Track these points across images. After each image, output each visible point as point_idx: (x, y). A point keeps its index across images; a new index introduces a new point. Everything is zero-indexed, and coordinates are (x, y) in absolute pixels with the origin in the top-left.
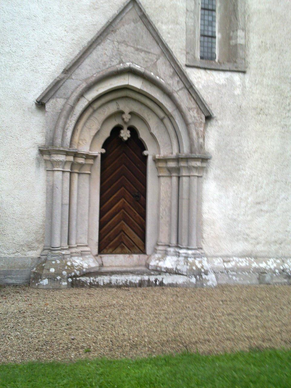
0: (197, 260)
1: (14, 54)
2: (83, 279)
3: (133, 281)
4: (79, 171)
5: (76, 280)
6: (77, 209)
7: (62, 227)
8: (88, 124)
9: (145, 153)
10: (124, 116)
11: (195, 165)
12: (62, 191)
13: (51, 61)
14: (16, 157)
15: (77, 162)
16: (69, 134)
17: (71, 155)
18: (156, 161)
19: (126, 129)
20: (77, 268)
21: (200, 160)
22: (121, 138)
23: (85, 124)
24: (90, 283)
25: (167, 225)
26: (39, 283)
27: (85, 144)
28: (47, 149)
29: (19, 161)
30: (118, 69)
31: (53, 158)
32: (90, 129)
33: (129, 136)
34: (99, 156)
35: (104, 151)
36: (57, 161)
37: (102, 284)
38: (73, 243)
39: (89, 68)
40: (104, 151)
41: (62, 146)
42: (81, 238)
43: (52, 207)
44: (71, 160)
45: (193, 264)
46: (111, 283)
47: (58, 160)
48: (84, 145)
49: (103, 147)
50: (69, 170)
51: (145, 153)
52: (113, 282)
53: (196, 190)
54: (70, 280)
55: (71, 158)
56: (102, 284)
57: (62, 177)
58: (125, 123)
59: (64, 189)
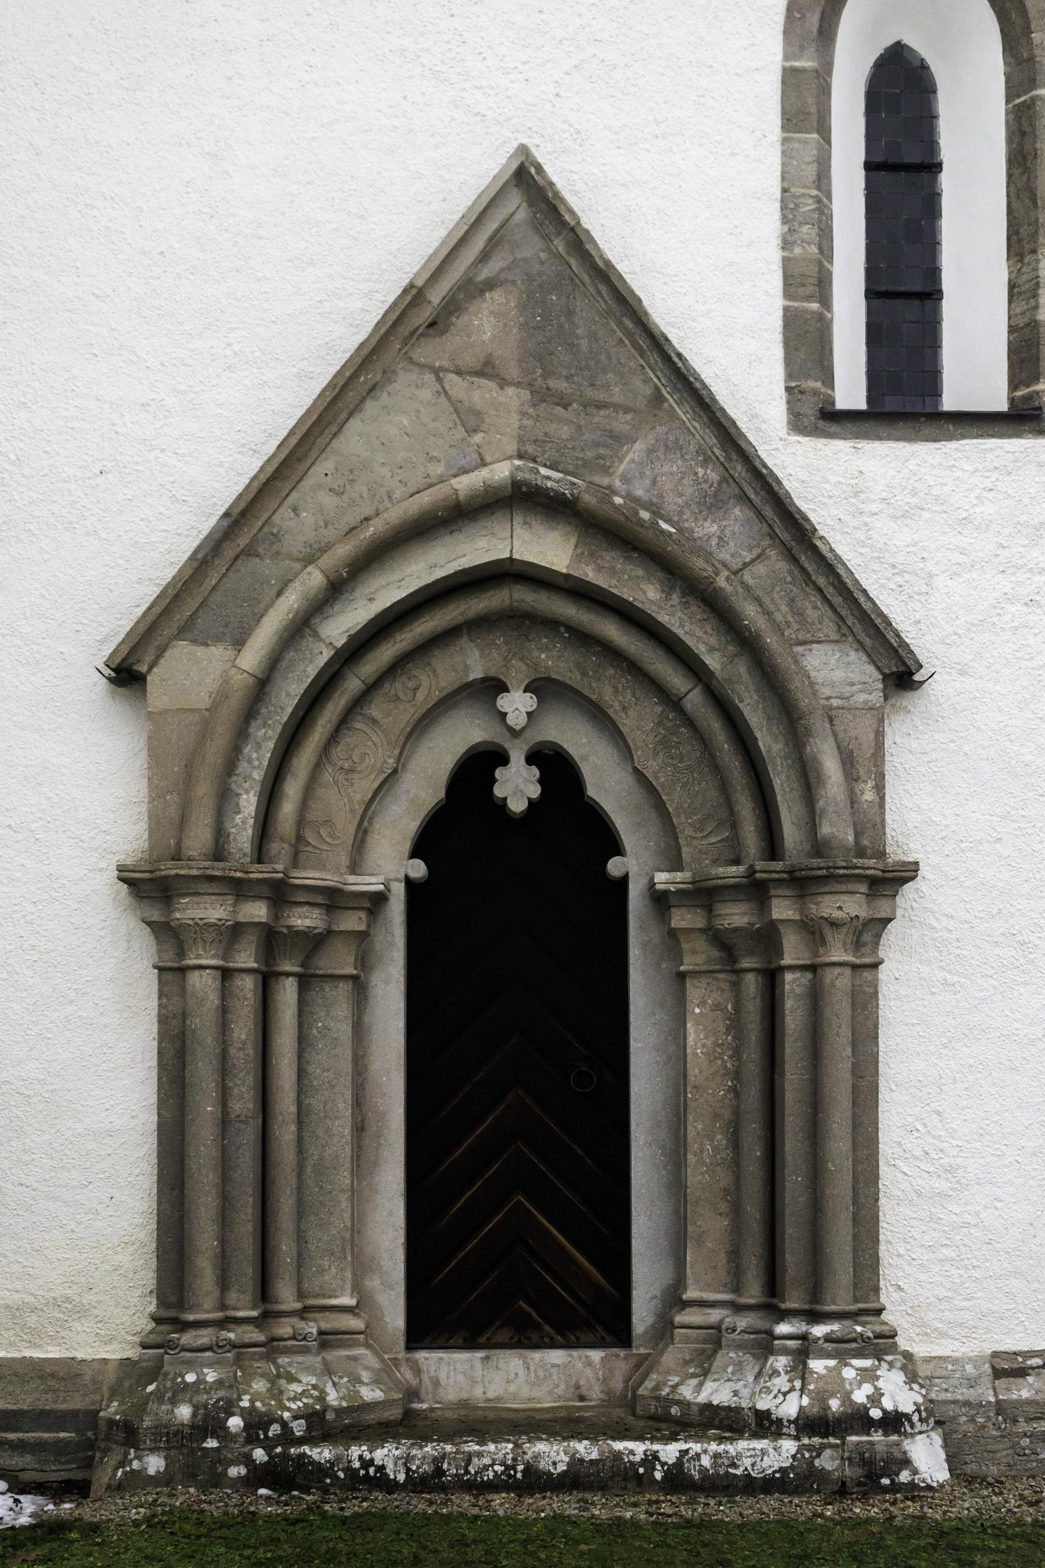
0: (852, 1366)
1: (13, 468)
2: (322, 1454)
3: (543, 1465)
4: (223, 959)
5: (285, 1455)
6: (300, 1140)
7: (225, 1219)
8: (338, 752)
9: (615, 867)
10: (504, 702)
11: (837, 914)
12: (224, 1057)
13: (168, 486)
14: (33, 917)
15: (289, 927)
16: (249, 803)
17: (258, 897)
18: (661, 901)
19: (523, 762)
20: (294, 1406)
21: (863, 888)
22: (502, 805)
23: (326, 750)
24: (349, 1470)
25: (724, 1207)
26: (128, 1469)
27: (329, 840)
28: (154, 875)
29: (44, 933)
30: (457, 498)
31: (178, 915)
32: (352, 770)
33: (535, 791)
34: (399, 890)
35: (418, 869)
36: (197, 924)
37: (401, 1477)
38: (287, 1297)
39: (329, 501)
40: (418, 869)
41: (176, 857)
42: (322, 1271)
43: (183, 1134)
44: (257, 920)
45: (835, 1384)
46: (439, 1472)
47: (201, 923)
48: (325, 847)
49: (416, 852)
50: (297, 969)
51: (615, 867)
52: (450, 1469)
53: (845, 1032)
54: (259, 1455)
55: (258, 911)
56: (401, 1477)
57: (223, 997)
58: (515, 733)
59: (232, 1051)
